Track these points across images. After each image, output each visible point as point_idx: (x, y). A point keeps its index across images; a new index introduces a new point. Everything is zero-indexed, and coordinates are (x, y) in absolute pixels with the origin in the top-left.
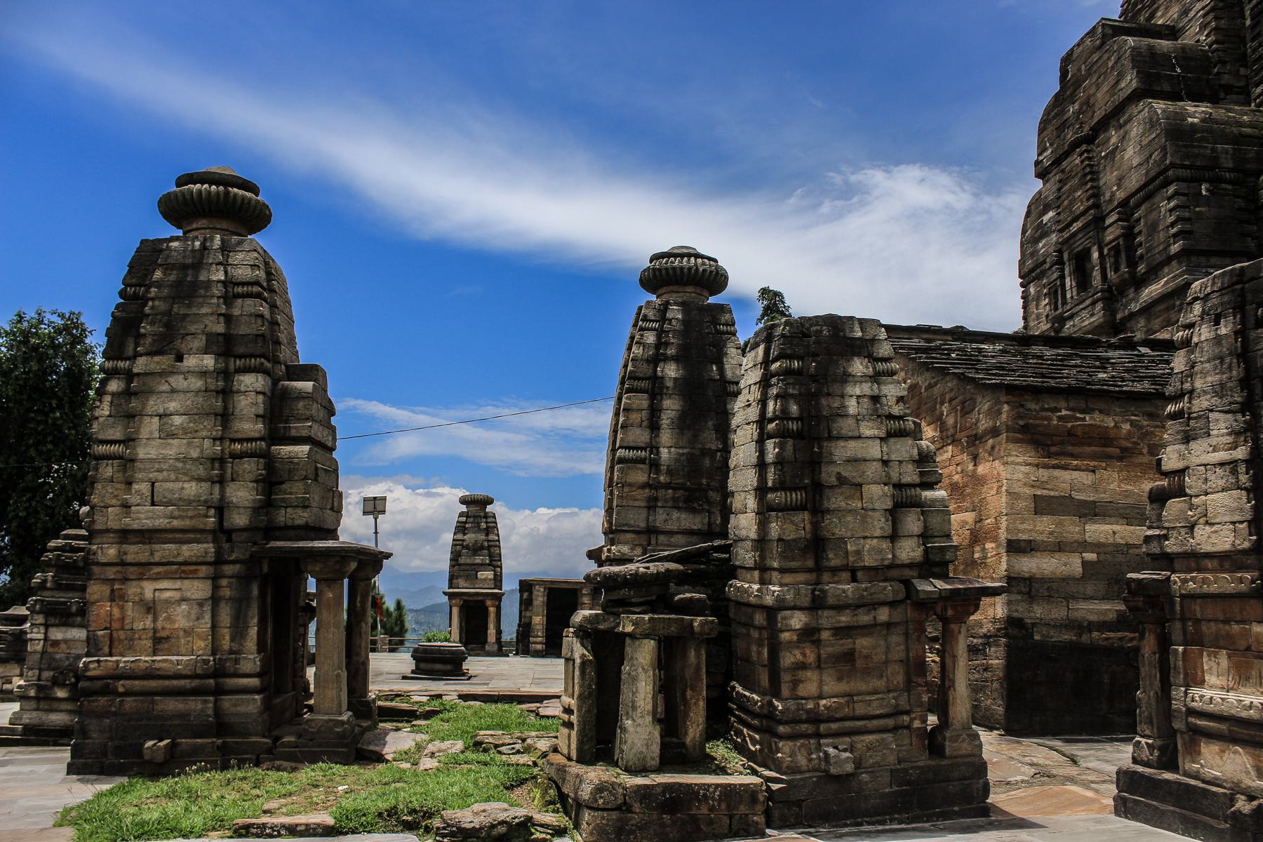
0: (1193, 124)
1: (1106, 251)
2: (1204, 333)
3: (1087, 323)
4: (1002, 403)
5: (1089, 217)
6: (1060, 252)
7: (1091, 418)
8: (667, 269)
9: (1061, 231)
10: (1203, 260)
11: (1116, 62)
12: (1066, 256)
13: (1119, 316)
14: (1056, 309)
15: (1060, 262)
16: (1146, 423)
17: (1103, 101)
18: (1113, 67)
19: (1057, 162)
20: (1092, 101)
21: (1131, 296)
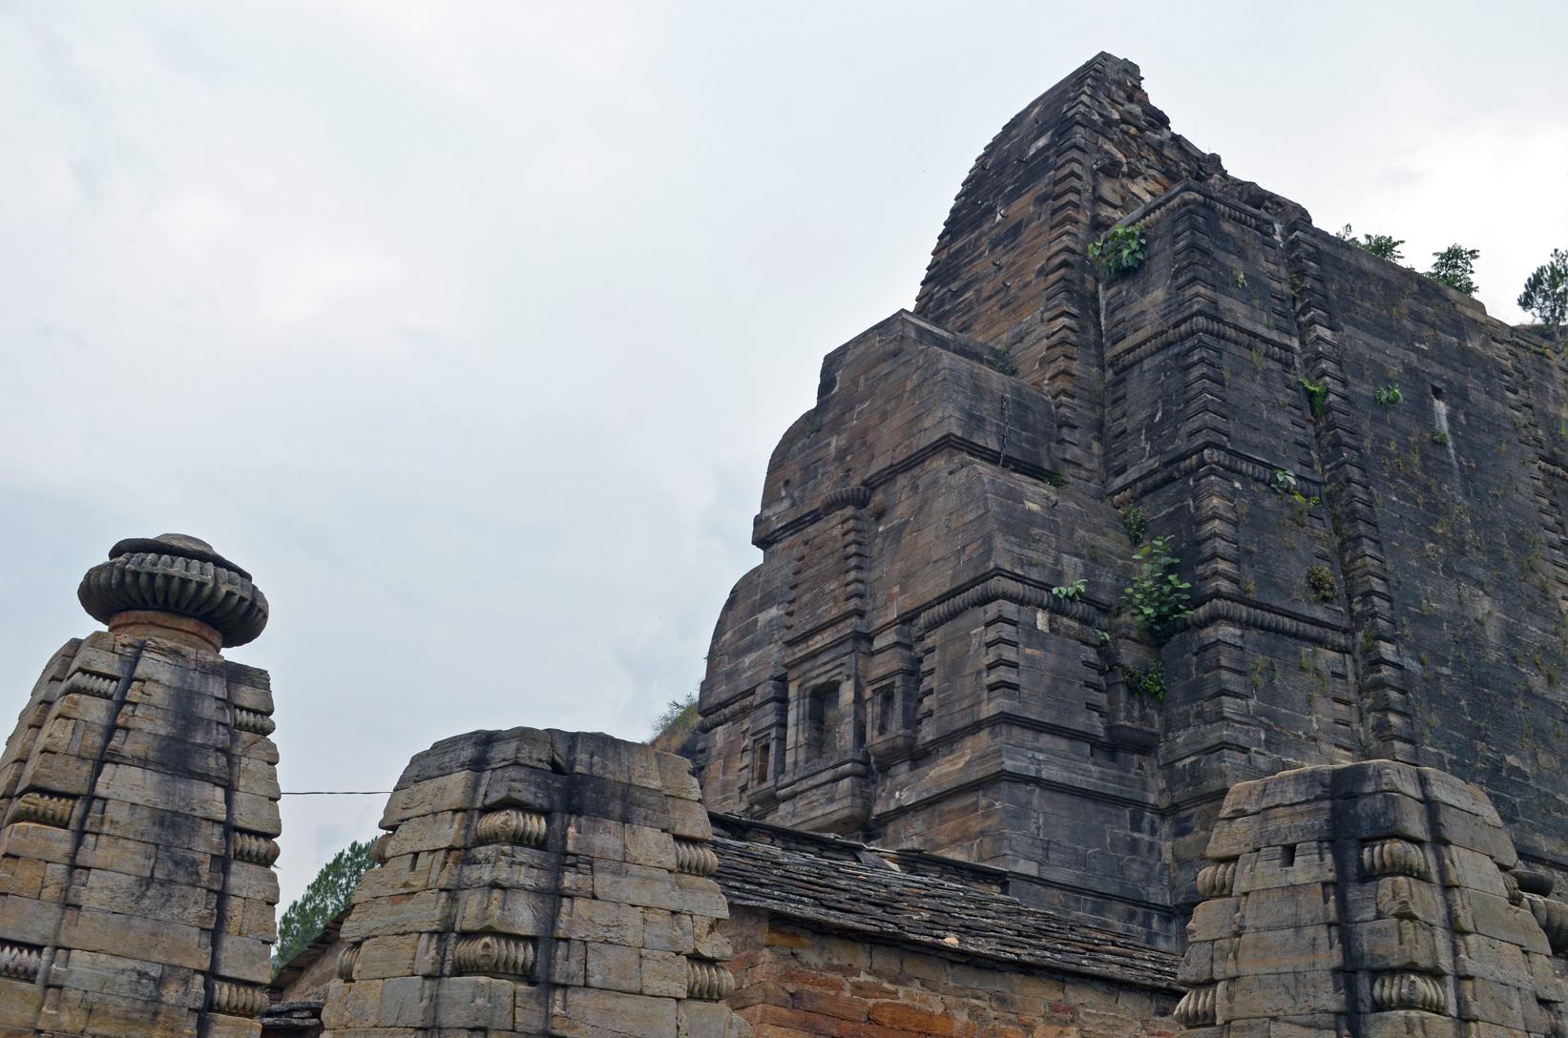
0: (1030, 512)
1: (868, 693)
2: (1260, 874)
3: (819, 812)
4: (758, 947)
5: (846, 628)
6: (782, 681)
7: (907, 994)
8: (152, 576)
9: (791, 644)
10: (1029, 735)
11: (920, 386)
12: (793, 691)
13: (878, 809)
14: (763, 779)
15: (782, 701)
16: (993, 1014)
17: (888, 446)
18: (913, 391)
19: (796, 525)
20: (870, 438)
21: (902, 778)
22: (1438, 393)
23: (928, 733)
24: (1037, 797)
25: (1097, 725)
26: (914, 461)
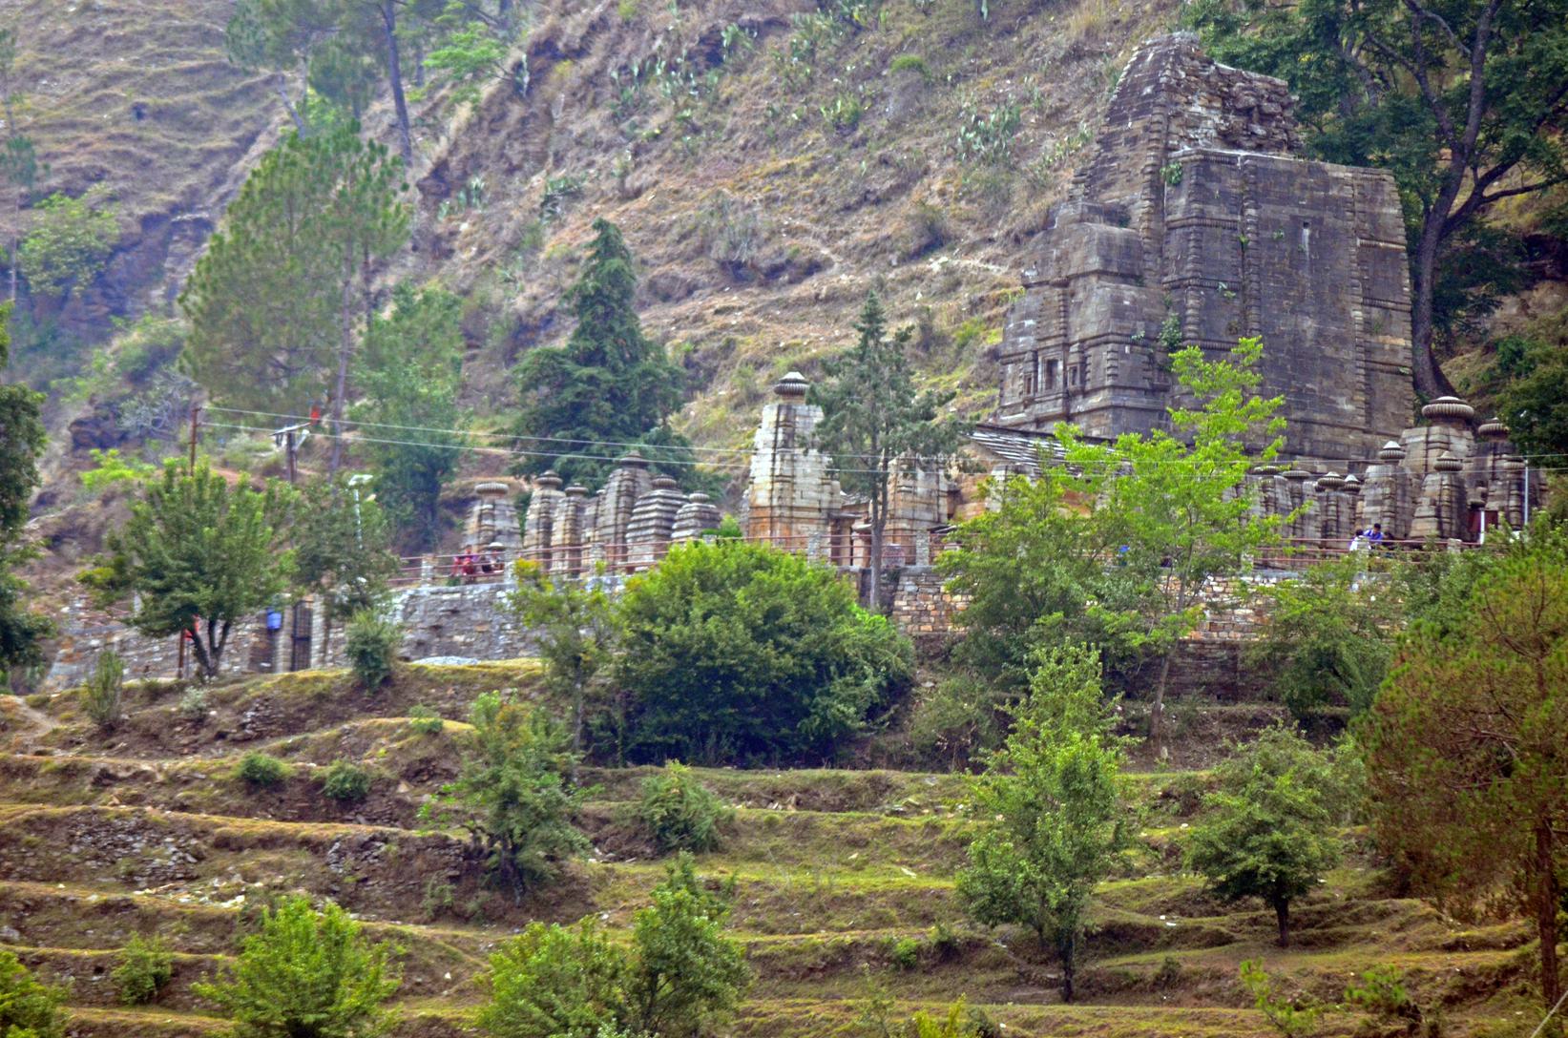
22: (1306, 225)
23: (1088, 386)
24: (1124, 412)
25: (1147, 384)
26: (1085, 275)
